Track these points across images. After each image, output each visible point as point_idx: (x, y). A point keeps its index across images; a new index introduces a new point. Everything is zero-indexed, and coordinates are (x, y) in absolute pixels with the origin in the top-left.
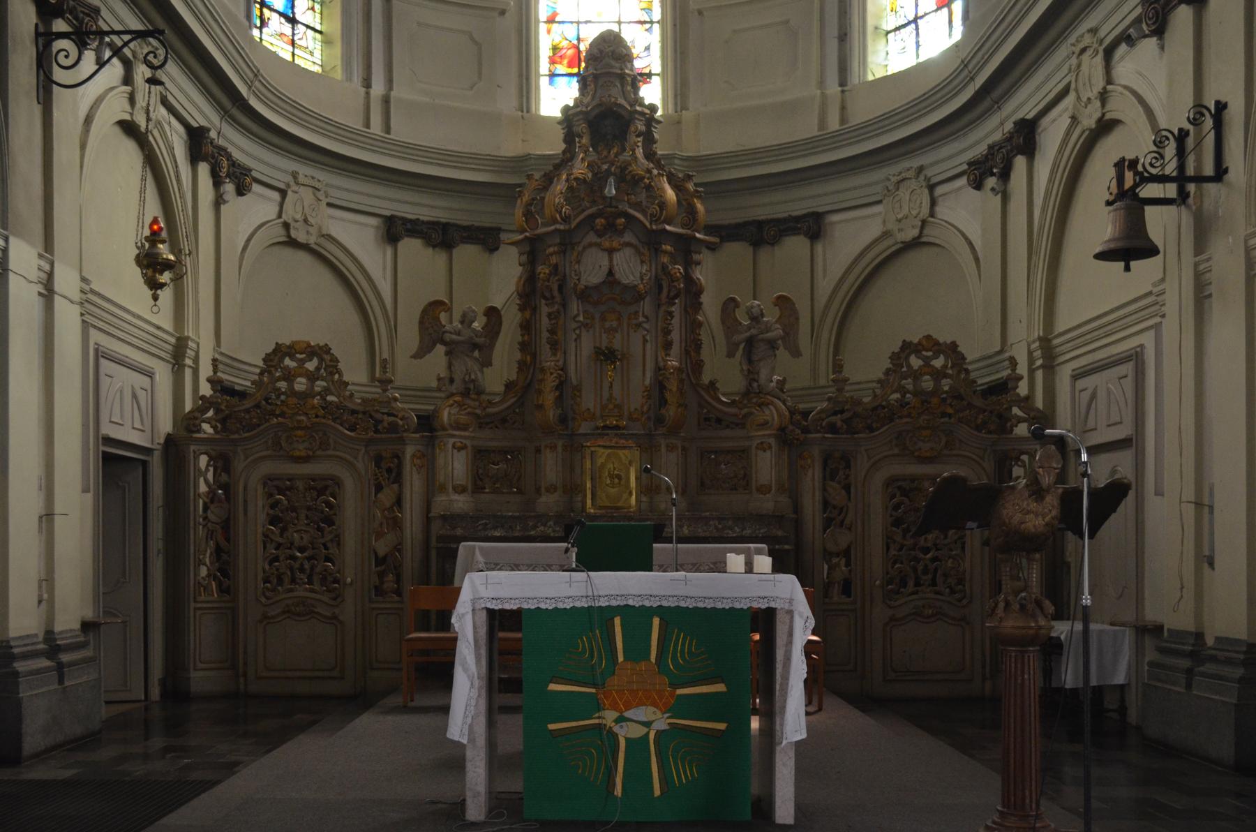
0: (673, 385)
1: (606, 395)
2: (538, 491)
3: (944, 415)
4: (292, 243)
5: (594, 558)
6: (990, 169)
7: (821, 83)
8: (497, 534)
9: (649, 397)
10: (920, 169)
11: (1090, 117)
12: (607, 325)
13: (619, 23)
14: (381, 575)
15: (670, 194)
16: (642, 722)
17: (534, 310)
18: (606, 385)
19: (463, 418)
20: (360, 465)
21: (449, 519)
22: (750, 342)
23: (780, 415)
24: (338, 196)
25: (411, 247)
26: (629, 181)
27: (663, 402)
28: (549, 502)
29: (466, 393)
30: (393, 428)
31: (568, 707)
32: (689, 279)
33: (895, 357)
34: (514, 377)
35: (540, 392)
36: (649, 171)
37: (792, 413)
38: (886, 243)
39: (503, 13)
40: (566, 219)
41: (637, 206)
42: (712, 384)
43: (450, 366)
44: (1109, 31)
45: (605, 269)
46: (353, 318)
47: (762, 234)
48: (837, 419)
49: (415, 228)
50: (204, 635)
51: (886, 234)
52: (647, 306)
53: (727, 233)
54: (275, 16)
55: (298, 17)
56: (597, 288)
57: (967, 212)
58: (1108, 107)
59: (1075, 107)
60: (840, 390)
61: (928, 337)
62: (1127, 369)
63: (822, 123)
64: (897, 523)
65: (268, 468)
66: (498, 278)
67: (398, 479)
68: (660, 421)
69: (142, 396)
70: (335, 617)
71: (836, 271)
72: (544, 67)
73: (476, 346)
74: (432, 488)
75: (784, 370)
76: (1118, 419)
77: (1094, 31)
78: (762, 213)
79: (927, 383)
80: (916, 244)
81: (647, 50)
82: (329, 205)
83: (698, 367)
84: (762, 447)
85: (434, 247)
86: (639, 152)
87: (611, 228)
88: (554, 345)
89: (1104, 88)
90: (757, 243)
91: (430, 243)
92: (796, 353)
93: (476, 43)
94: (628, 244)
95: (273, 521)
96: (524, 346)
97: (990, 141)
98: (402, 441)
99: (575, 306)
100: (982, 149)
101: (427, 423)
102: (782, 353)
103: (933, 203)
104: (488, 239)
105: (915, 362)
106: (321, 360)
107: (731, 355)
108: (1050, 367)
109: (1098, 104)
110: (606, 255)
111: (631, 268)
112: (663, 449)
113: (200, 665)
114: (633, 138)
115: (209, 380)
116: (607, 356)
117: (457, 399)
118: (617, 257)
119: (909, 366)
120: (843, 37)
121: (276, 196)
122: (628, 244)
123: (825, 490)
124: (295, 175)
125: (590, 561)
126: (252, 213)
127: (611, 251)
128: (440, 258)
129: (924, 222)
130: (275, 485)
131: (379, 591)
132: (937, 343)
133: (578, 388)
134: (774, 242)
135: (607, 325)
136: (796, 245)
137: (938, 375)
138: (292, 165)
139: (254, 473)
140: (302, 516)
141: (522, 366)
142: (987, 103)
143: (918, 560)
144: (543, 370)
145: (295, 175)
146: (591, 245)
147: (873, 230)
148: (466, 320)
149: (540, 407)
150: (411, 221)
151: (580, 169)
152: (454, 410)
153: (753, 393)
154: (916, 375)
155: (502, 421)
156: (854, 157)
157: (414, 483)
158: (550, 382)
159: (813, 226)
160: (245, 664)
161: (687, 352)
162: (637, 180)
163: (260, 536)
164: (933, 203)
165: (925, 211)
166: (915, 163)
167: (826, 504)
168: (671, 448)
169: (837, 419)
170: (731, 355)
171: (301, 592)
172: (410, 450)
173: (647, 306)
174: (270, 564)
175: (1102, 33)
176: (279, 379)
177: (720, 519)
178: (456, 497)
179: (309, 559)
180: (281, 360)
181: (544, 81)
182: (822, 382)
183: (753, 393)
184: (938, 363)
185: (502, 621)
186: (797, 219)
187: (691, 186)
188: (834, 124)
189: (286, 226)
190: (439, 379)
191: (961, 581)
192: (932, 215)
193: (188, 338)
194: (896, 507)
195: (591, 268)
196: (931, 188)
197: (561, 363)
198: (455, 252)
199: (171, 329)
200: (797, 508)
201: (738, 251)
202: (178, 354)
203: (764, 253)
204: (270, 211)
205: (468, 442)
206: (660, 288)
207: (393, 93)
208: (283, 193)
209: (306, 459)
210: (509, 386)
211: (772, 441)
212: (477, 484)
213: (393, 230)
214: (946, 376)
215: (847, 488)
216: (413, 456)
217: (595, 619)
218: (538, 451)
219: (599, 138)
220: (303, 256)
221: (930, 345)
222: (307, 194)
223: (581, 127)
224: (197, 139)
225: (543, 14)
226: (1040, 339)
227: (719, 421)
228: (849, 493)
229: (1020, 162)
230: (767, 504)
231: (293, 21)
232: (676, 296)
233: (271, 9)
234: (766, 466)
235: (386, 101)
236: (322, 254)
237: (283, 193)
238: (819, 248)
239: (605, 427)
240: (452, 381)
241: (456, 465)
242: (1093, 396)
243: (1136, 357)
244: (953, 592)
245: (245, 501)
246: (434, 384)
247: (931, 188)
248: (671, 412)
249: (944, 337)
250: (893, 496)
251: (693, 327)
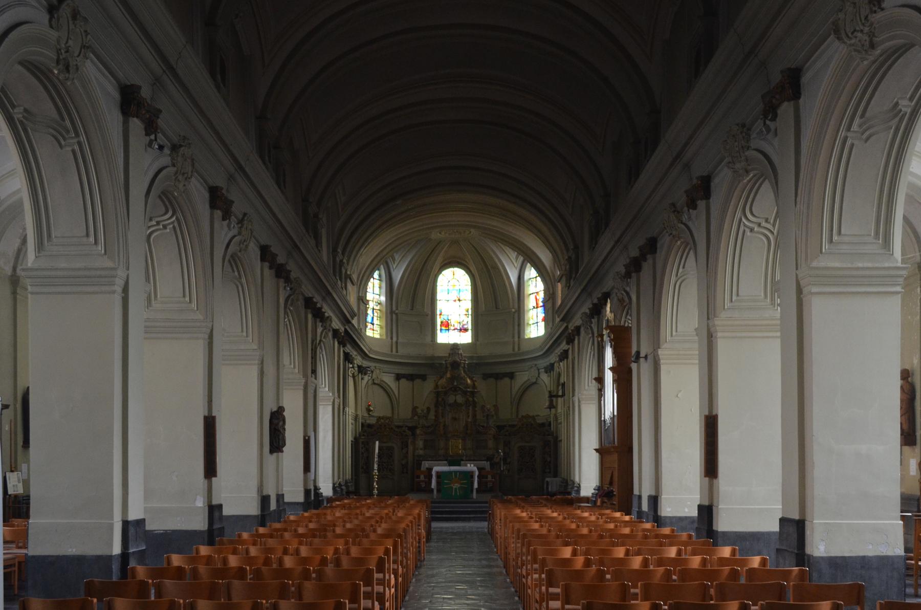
4: (375, 384)
5: (451, 464)
7: (513, 337)
15: (469, 381)
16: (456, 486)
28: (441, 452)
31: (447, 484)
46: (385, 395)
47: (498, 377)
63: (514, 350)
66: (428, 387)
67: (407, 447)
71: (517, 388)
72: (439, 327)
80: (535, 383)
91: (408, 379)
96: (436, 416)
111: (460, 399)
116: (455, 419)
120: (519, 325)
125: (450, 465)
134: (501, 379)
136: (507, 380)
157: (411, 448)
159: (511, 376)
181: (438, 331)
185: (437, 473)
195: (451, 399)
198: (415, 382)
212: (425, 448)
213: (398, 377)
217: (450, 472)
221: (528, 416)
225: (438, 313)
234: (491, 444)
236: (382, 386)
241: (420, 444)
249: (531, 414)
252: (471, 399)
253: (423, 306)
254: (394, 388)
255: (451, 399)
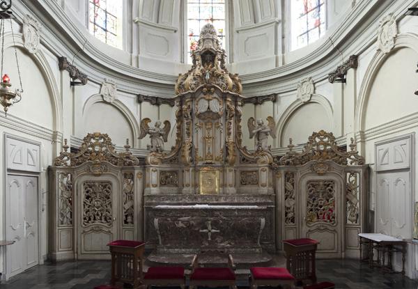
0: (231, 148)
1: (207, 152)
2: (183, 186)
3: (328, 158)
4: (105, 102)
6: (339, 77)
7: (276, 52)
8: (167, 202)
9: (223, 152)
10: (311, 78)
11: (387, 48)
12: (207, 127)
13: (212, 20)
14: (126, 216)
15: (230, 81)
17: (182, 122)
18: (207, 148)
19: (156, 161)
20: (119, 178)
21: (151, 197)
22: (258, 133)
23: (270, 159)
24: (120, 87)
25: (145, 104)
26: (215, 76)
27: (228, 154)
29: (157, 151)
30: (130, 164)
32: (237, 111)
33: (310, 138)
34: (174, 145)
35: (183, 151)
36: (222, 72)
37: (274, 158)
38: (299, 102)
39: (175, 31)
40: (193, 89)
41: (218, 85)
42: (245, 147)
43: (151, 142)
44: (398, 14)
45: (207, 107)
46: (127, 127)
47: (258, 101)
48: (290, 160)
49: (147, 99)
50: (62, 237)
51: (298, 100)
52: (222, 120)
53: (246, 101)
54: (99, 29)
55: (108, 29)
56: (203, 113)
57: (328, 91)
58: (397, 43)
59: (380, 45)
60: (291, 150)
61: (322, 131)
62: (407, 141)
63: (277, 65)
64: (311, 197)
65: (85, 178)
68: (226, 161)
69: (34, 153)
70: (110, 232)
73: (161, 135)
74: (145, 185)
75: (268, 142)
76: (400, 160)
77: (391, 14)
78: (258, 94)
79: (322, 148)
81: (220, 26)
82: (118, 90)
83: (240, 141)
84: (263, 170)
85: (153, 104)
86: (219, 66)
87: (209, 91)
88: (188, 134)
89: (396, 35)
90: (256, 104)
92: (274, 137)
93: (167, 41)
94: (215, 98)
95: (88, 197)
96: (178, 135)
97: (339, 65)
98: (133, 169)
99: (196, 120)
100: (335, 68)
101: (143, 161)
102: (270, 137)
103: (315, 89)
104: (170, 102)
105: (318, 140)
106: (105, 139)
107: (251, 137)
108: (363, 142)
109: (393, 42)
110: (207, 101)
111: (216, 106)
112: (228, 171)
113: (60, 250)
114: (216, 61)
115: (350, 146)
117: (154, 153)
118: (211, 102)
119: (316, 141)
121: (99, 86)
122: (215, 98)
123: (285, 185)
124: (105, 79)
126: (87, 92)
127: (209, 100)
128: (156, 108)
129: (311, 95)
130: (312, 184)
131: (126, 222)
132: (325, 133)
133: (197, 149)
135: (207, 127)
136: (269, 104)
137: (326, 144)
138: (104, 76)
139: (81, 180)
140: (98, 195)
141: (177, 141)
142: (338, 51)
143: (318, 210)
144: (184, 143)
145: (105, 79)
146: (202, 98)
147: (294, 98)
148: (157, 125)
149: (183, 156)
150: (146, 96)
151: (198, 71)
152: (152, 157)
153: (259, 151)
154: (318, 145)
155: (171, 161)
156: (282, 77)
157: (138, 184)
158: (187, 147)
159: (274, 98)
160: (77, 249)
161: (236, 137)
162: (218, 76)
163: (82, 203)
164: (315, 89)
165: (312, 92)
166: (309, 76)
167: (286, 190)
168: (230, 171)
169: (290, 160)
170: (251, 137)
171: (97, 222)
172: (136, 172)
173: (222, 120)
174: (86, 213)
175: (395, 15)
176: (89, 147)
177: (248, 196)
178: (152, 188)
179: (100, 211)
180: (90, 140)
182: (277, 147)
183: (259, 151)
184: (326, 140)
186: (269, 96)
187: (237, 78)
188: (280, 64)
189: (102, 96)
190: (148, 146)
191: (334, 218)
192: (314, 93)
193: (57, 132)
194: (310, 191)
195: (202, 106)
196: (314, 84)
197: (191, 141)
199: (51, 129)
200: (275, 191)
201: (250, 106)
202: (54, 139)
203: (258, 106)
204: (97, 91)
205: (158, 169)
206: (227, 113)
207: (140, 55)
208: (101, 85)
209: (99, 175)
210: (173, 148)
211: (267, 168)
213: (140, 99)
214: (329, 145)
215: (293, 184)
216: (138, 174)
218: (183, 172)
219: (204, 61)
220: (108, 106)
221: (322, 134)
222: (109, 86)
223: (198, 57)
224: (62, 62)
226: (360, 132)
227: (247, 161)
228: (293, 186)
229: (351, 71)
230: (265, 190)
231: (106, 30)
232: (233, 116)
233: (98, 25)
234: (265, 177)
235: (137, 58)
237: (101, 85)
238: (276, 105)
239: (207, 163)
240: (152, 147)
241: (154, 177)
242: (387, 152)
243: (411, 137)
244: (331, 221)
245: (77, 190)
246: (146, 148)
247: (314, 84)
248: (230, 158)
249: (328, 131)
250: (309, 187)
251: (238, 128)
252: (233, 107)
253: (171, 19)
254: (134, 113)
255: (202, 106)
